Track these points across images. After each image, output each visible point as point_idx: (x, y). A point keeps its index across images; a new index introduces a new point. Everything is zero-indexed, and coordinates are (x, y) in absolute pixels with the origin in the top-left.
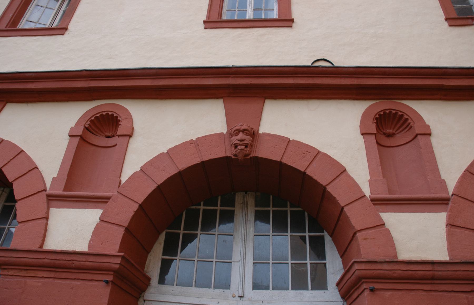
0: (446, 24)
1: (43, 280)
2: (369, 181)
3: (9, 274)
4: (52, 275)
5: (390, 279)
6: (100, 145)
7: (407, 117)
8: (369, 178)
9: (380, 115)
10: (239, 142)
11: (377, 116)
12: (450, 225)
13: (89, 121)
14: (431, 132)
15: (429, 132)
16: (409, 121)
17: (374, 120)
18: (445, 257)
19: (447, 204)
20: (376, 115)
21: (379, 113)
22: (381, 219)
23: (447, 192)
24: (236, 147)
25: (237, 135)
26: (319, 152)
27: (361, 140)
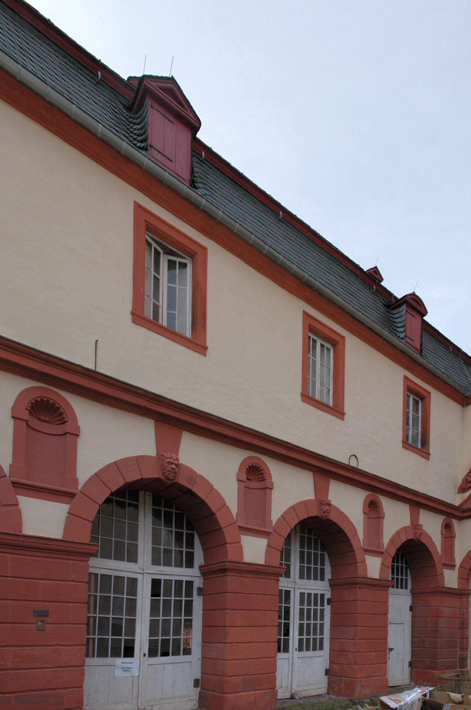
0: (130, 317)
1: (250, 579)
2: (10, 465)
3: (232, 575)
4: (253, 576)
5: (38, 549)
6: (33, 427)
7: (63, 411)
8: (11, 462)
9: (36, 401)
10: (326, 511)
11: (33, 401)
12: (268, 545)
13: (46, 399)
14: (79, 433)
15: (77, 434)
16: (64, 416)
17: (30, 404)
18: (263, 562)
19: (73, 497)
20: (32, 400)
21: (36, 399)
22: (17, 500)
23: (77, 489)
24: (324, 512)
25: (326, 506)
26: (466, 556)
27: (11, 423)
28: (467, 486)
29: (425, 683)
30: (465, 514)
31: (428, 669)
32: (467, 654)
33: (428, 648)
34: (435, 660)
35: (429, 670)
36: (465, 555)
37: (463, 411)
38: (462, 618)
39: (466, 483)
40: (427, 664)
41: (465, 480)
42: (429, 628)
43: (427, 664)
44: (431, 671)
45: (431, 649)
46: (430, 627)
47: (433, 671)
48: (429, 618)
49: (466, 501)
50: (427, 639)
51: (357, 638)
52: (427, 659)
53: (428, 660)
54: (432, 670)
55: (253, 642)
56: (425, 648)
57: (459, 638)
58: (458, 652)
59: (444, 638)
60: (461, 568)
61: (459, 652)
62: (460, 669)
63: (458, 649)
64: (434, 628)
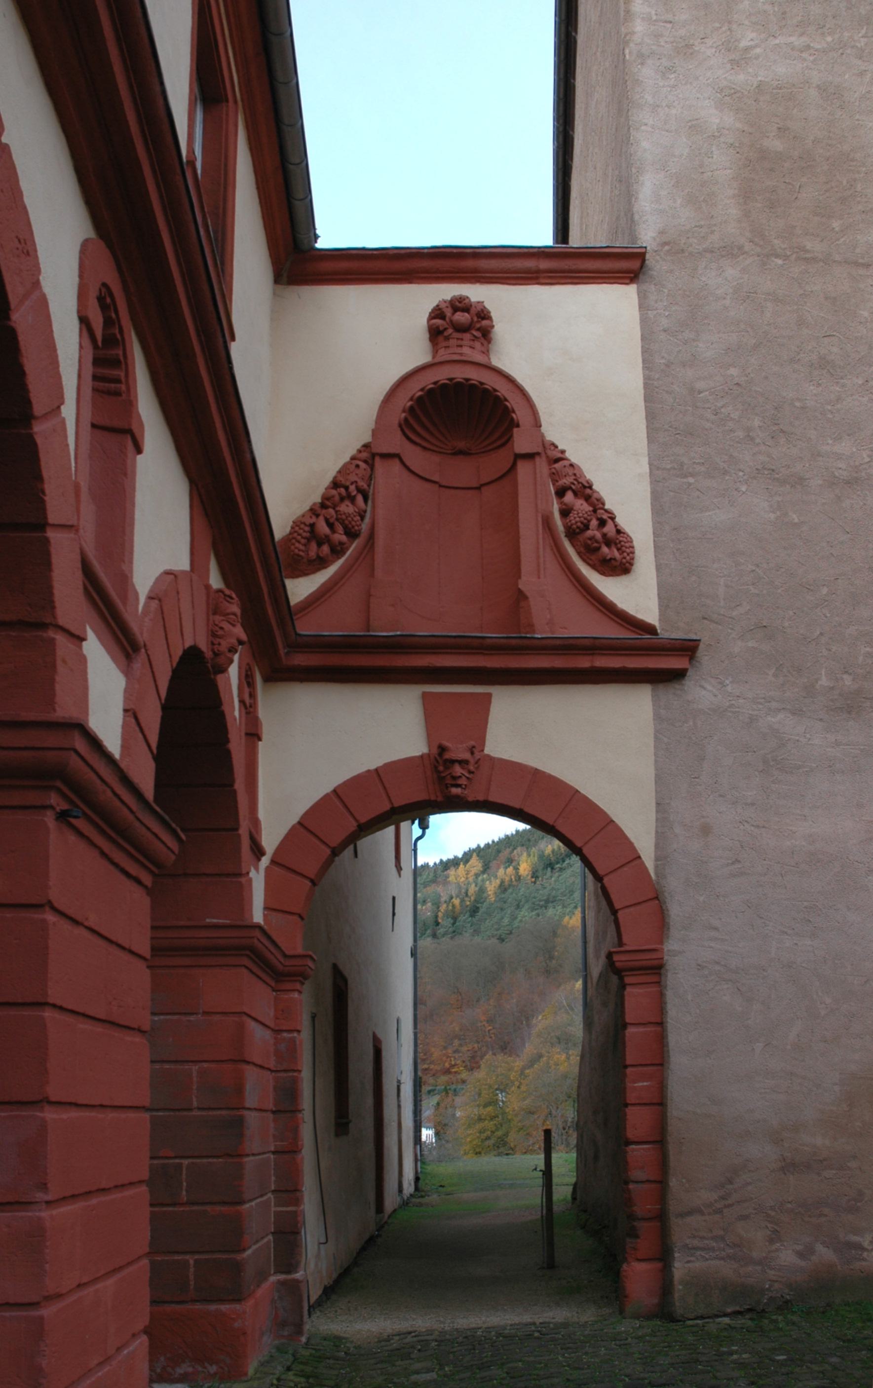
26: (299, 823)
28: (313, 554)
29: (185, 1368)
30: (300, 660)
31: (194, 1301)
32: (304, 1209)
33: (193, 1204)
34: (232, 1256)
35: (198, 1306)
36: (294, 819)
37: (274, 294)
38: (285, 1071)
39: (309, 540)
40: (192, 1277)
41: (307, 529)
42: (196, 1113)
43: (192, 1277)
44: (213, 1307)
45: (208, 1208)
46: (199, 1109)
47: (224, 1307)
48: (195, 1068)
49: (336, 584)
50: (186, 1162)
51: (40, 1196)
52: (187, 1257)
53: (191, 1260)
54: (222, 1301)
55: (76, 1105)
56: (174, 1204)
57: (274, 1153)
58: (273, 1209)
59: (253, 1155)
60: (276, 868)
61: (276, 1206)
62: (282, 1277)
63: (270, 1195)
64: (224, 1112)
